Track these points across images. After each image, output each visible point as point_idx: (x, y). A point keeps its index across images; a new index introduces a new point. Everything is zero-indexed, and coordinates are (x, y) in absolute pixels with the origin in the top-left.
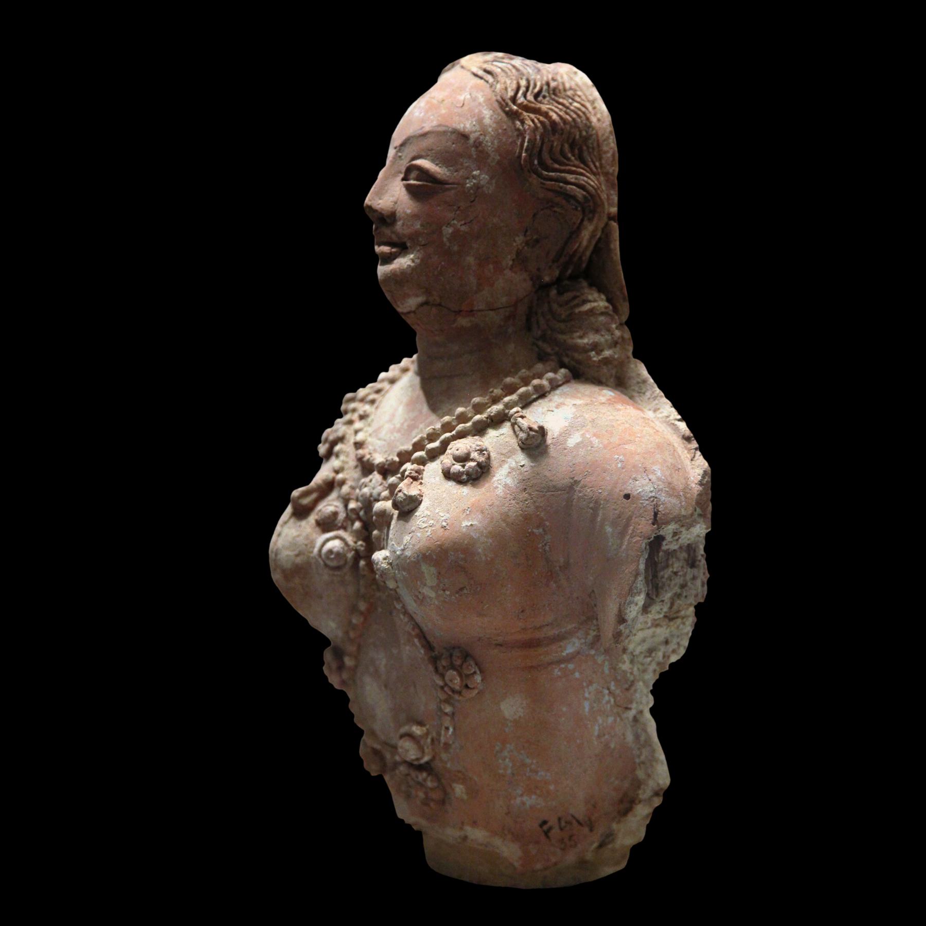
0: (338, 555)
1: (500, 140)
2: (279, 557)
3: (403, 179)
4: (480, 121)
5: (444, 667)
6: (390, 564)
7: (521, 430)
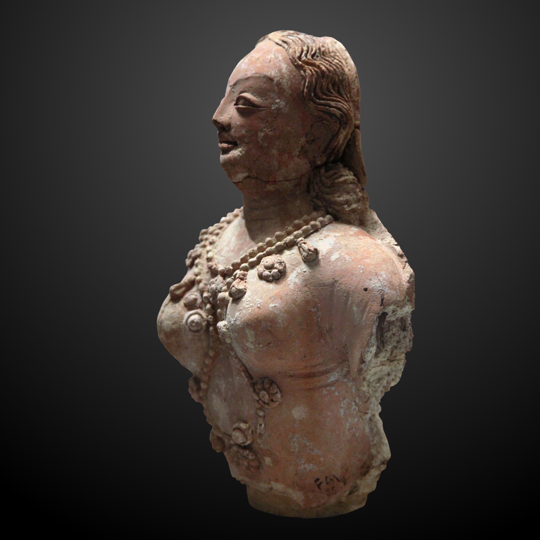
0: (197, 324)
1: (292, 82)
2: (163, 325)
3: (235, 105)
4: (280, 70)
5: (259, 389)
6: (228, 329)
7: (304, 251)
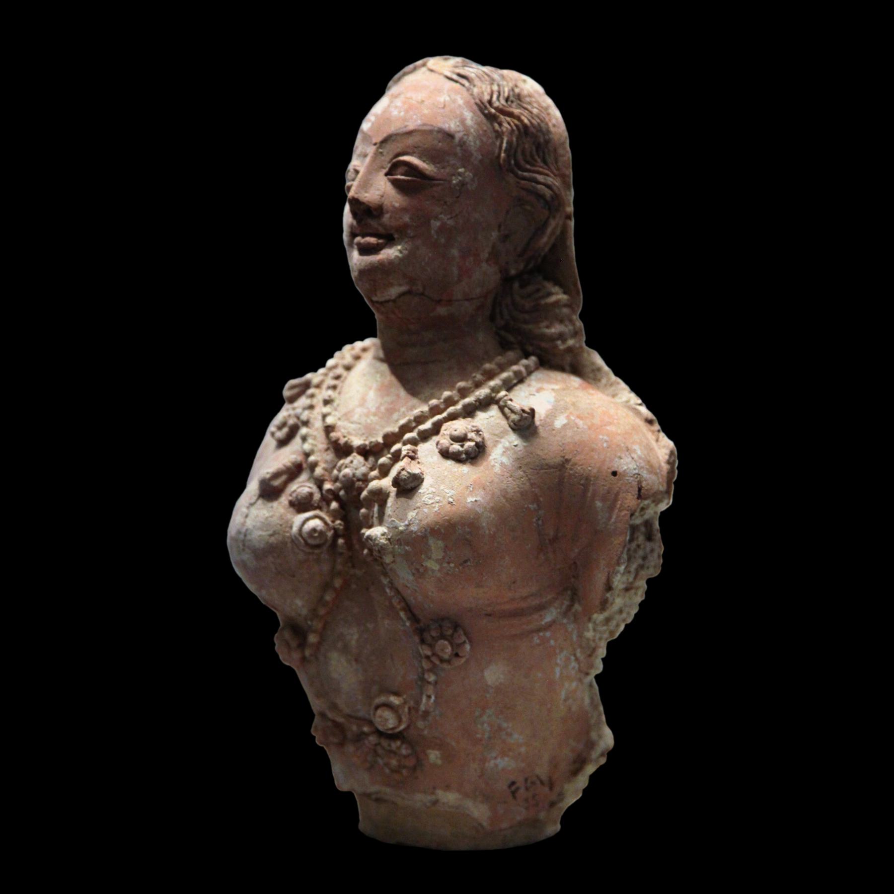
0: (321, 533)
1: (482, 141)
2: (249, 537)
3: (386, 175)
4: (463, 121)
5: (433, 637)
6: (389, 540)
7: (513, 411)
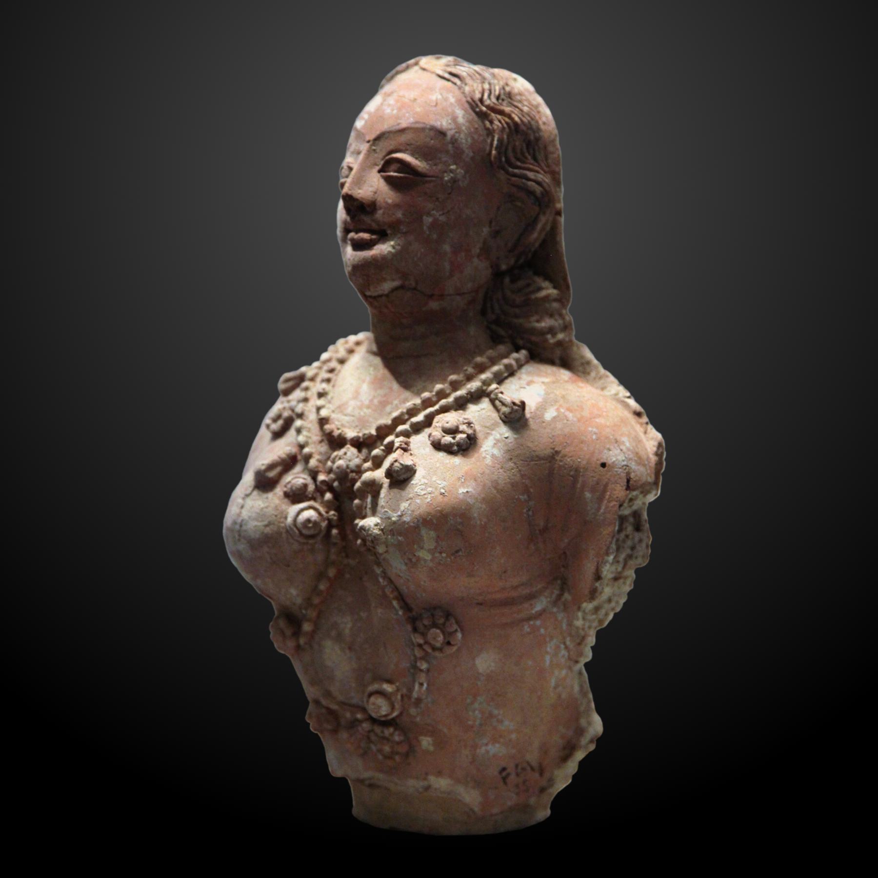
0: (316, 523)
1: (473, 138)
2: (244, 528)
3: (379, 171)
4: (454, 119)
5: (425, 626)
6: (382, 530)
7: (503, 404)
